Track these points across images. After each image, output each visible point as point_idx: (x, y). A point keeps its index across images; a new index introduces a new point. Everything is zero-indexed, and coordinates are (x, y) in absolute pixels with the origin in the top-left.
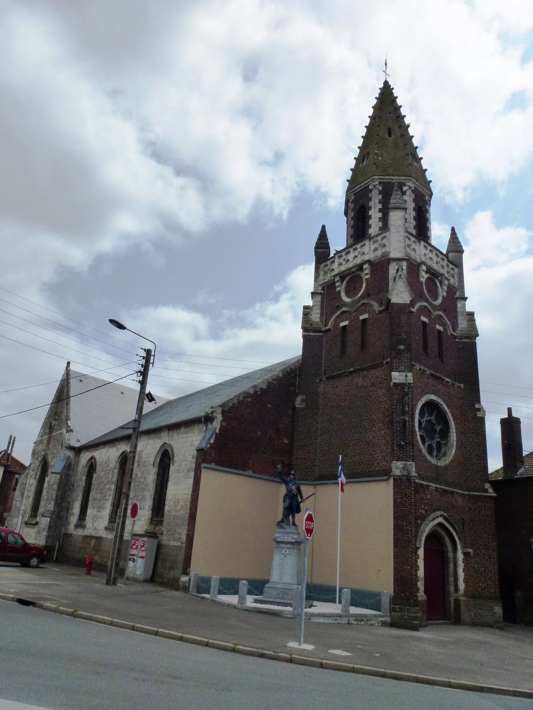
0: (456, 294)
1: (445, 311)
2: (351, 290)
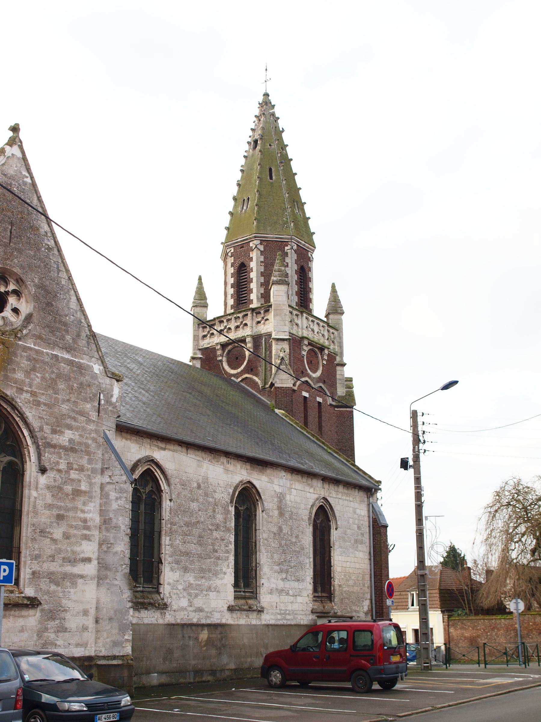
0: (334, 363)
1: (324, 382)
2: (235, 361)
